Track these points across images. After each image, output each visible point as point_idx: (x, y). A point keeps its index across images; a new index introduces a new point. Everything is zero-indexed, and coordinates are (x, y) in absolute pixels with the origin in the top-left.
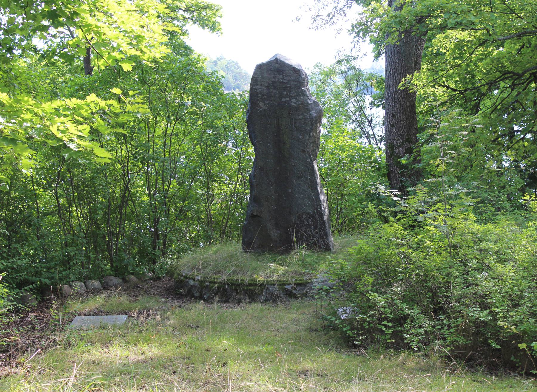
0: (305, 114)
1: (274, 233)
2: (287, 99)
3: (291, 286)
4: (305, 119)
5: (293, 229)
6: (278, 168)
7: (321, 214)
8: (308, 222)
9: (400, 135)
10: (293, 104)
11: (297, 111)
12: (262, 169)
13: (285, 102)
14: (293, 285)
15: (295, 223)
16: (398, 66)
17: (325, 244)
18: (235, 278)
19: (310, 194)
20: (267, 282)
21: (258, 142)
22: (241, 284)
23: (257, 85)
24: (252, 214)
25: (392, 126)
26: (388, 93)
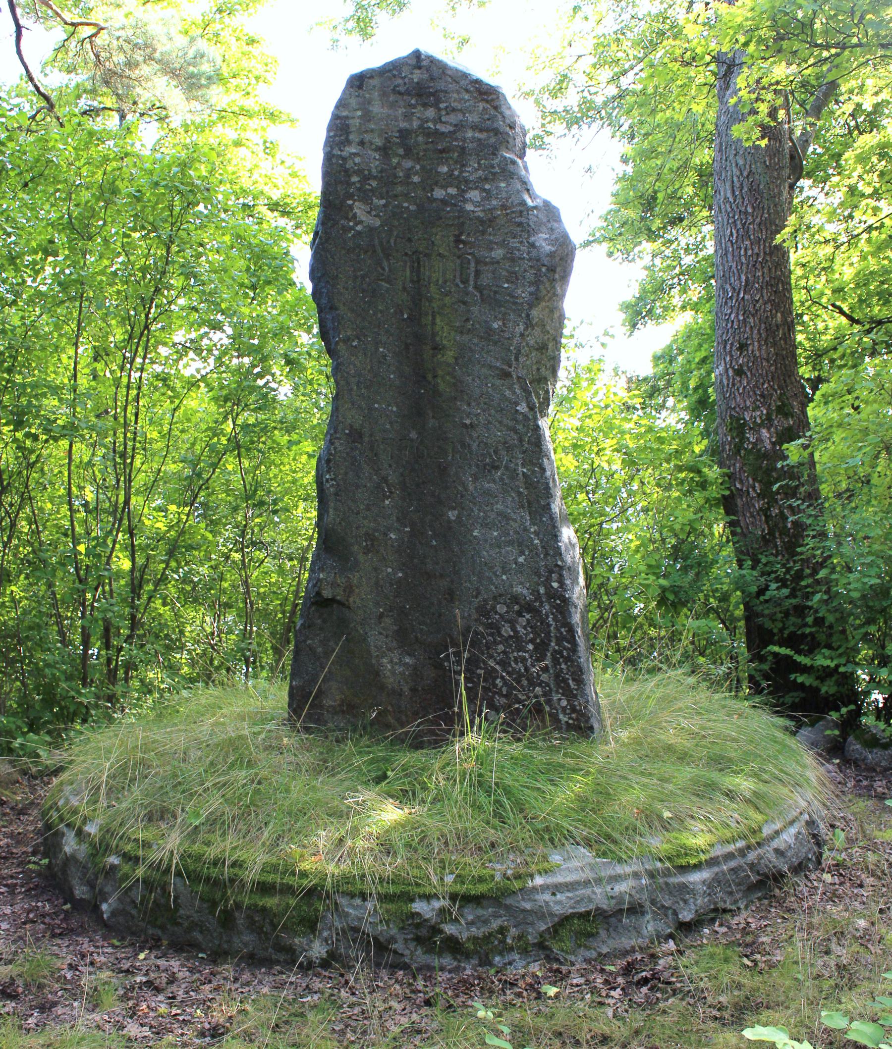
0: (514, 243)
1: (394, 666)
2: (452, 191)
3: (437, 904)
4: (513, 260)
5: (458, 654)
6: (413, 435)
7: (563, 605)
8: (514, 629)
9: (762, 396)
10: (469, 207)
11: (483, 233)
12: (355, 435)
13: (444, 202)
14: (444, 903)
15: (467, 629)
16: (753, 223)
17: (574, 710)
18: (211, 853)
19: (526, 530)
20: (336, 886)
21: (346, 340)
22: (232, 881)
23: (348, 142)
24: (318, 594)
25: (739, 372)
26: (725, 291)
